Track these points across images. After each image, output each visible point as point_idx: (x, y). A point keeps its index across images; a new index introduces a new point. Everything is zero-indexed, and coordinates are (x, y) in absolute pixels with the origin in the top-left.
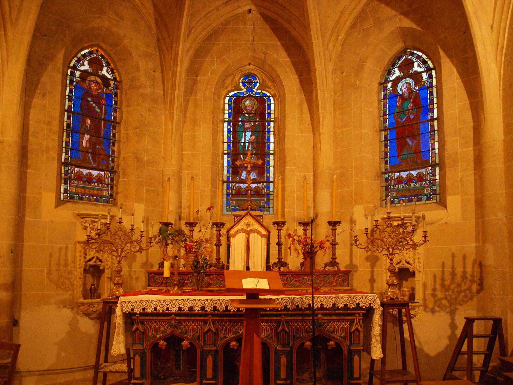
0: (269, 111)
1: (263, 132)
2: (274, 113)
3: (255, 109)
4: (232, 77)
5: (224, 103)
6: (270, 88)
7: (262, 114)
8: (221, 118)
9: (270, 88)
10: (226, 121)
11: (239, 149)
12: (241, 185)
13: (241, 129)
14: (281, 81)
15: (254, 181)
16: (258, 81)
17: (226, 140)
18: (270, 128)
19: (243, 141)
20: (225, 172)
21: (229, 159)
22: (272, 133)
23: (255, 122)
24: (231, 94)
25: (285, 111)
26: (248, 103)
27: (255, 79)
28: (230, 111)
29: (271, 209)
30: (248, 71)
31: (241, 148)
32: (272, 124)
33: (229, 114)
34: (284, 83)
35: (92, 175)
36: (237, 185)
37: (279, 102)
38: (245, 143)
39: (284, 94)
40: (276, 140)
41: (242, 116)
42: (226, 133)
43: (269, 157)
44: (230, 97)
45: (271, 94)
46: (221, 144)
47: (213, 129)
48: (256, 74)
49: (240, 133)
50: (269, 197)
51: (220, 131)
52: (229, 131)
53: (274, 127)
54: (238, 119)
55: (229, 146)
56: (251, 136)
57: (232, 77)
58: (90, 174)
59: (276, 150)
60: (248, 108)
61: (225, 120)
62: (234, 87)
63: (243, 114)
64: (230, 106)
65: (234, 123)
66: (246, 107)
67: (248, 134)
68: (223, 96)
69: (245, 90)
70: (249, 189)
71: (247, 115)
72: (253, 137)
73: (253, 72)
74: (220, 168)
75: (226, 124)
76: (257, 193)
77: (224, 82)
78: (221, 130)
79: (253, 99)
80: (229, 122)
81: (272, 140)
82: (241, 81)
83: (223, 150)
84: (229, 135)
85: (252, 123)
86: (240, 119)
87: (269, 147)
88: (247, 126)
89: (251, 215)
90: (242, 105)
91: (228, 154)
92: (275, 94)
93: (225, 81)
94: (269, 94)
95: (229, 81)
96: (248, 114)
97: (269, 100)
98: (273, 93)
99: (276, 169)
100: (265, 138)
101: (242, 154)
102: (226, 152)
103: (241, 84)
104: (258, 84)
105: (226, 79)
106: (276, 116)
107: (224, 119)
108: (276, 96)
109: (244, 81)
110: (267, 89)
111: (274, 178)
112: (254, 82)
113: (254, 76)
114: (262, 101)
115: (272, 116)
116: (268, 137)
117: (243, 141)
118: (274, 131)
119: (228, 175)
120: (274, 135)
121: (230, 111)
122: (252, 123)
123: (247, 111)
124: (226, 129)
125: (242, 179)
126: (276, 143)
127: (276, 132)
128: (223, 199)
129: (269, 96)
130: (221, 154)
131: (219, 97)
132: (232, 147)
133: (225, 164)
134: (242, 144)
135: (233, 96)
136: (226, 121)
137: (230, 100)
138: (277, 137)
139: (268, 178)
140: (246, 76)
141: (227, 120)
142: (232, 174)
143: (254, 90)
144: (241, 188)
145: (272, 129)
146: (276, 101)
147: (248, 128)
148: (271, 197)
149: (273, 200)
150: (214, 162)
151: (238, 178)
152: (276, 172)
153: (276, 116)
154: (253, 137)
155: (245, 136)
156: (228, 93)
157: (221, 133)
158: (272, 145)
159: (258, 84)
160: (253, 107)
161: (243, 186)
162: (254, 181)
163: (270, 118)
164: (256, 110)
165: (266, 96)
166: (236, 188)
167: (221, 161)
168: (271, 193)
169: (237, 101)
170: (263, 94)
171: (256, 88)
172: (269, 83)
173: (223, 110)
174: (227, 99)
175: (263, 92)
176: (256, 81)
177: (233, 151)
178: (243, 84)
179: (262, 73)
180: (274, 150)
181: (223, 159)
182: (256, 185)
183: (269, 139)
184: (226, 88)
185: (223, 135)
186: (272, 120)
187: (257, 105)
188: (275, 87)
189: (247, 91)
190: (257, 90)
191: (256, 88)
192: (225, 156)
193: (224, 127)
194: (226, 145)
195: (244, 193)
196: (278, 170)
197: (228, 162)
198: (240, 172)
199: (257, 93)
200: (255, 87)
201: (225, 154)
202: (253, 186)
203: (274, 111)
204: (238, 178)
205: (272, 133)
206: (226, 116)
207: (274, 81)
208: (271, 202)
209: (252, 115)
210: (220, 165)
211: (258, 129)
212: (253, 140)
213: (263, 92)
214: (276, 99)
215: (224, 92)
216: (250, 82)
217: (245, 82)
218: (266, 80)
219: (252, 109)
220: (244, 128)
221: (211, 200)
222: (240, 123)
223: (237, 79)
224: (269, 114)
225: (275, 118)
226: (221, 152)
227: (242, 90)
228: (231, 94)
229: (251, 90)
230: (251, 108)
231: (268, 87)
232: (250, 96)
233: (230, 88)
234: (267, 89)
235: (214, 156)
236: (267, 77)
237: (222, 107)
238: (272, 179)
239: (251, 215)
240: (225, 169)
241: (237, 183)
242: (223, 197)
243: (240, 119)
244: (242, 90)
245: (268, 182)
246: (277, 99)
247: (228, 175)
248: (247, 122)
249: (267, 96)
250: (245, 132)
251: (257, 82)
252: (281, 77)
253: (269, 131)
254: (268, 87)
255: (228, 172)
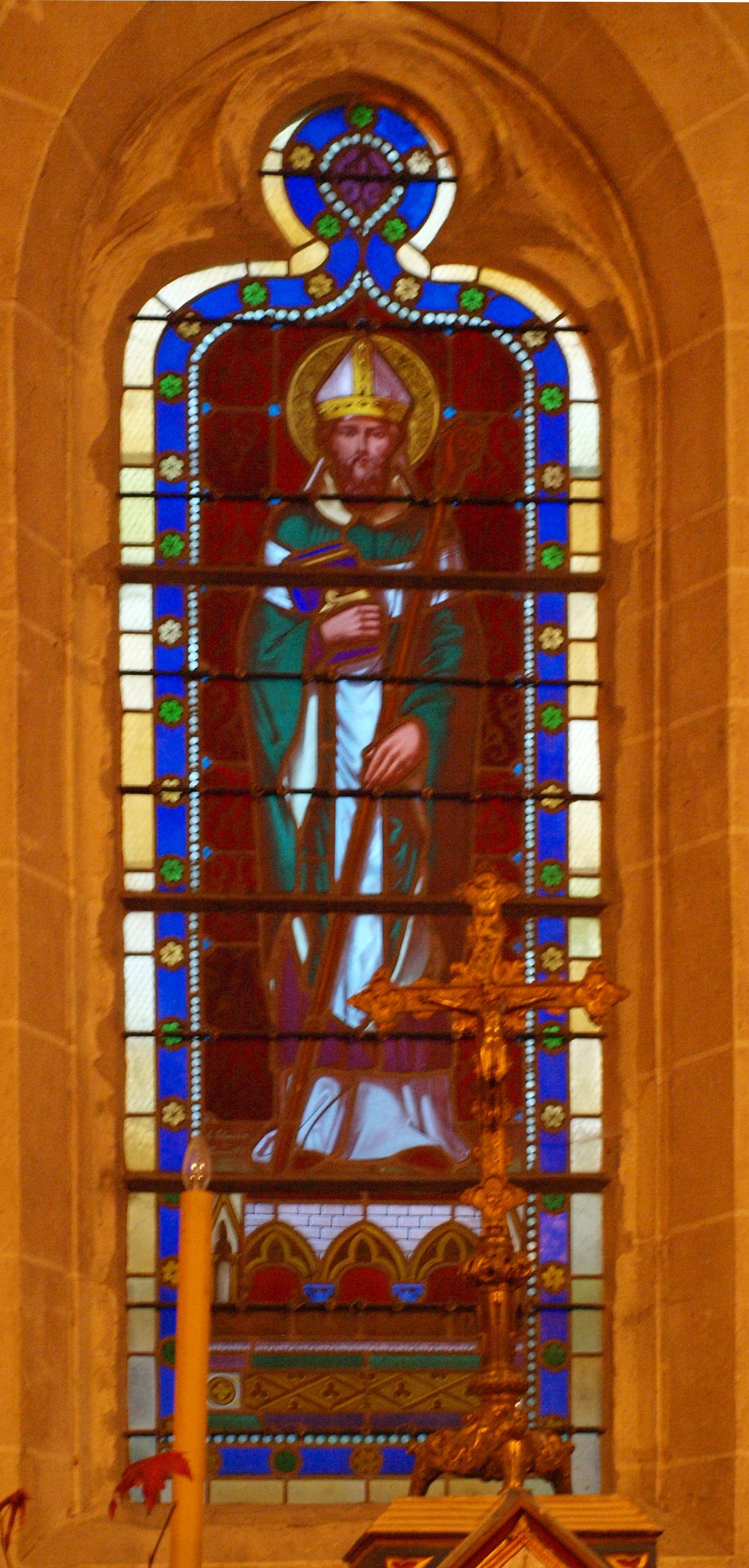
0: (552, 477)
1: (502, 688)
2: (603, 501)
3: (416, 452)
4: (188, 115)
5: (117, 389)
6: (566, 246)
7: (480, 504)
8: (93, 538)
9: (568, 247)
10: (135, 575)
11: (271, 851)
12: (302, 1217)
13: (291, 659)
14: (679, 181)
15: (417, 1178)
16: (445, 170)
17: (138, 767)
18: (561, 654)
19: (305, 774)
20: (141, 1092)
21: (173, 954)
22: (583, 700)
23: (417, 584)
24: (180, 292)
25: (718, 485)
26: (348, 387)
27: (411, 143)
28: (172, 468)
29: (585, 1448)
30: (343, 62)
31: (287, 845)
32: (582, 613)
33: (168, 499)
34: (715, 191)
35: (386, 1245)
36: (258, 1215)
37: (647, 384)
38: (324, 795)
39: (711, 312)
40: (625, 767)
41: (294, 525)
42: (138, 693)
43: (562, 942)
44: (173, 320)
45: (568, 305)
46: (98, 803)
47: (27, 647)
48: (422, 88)
49: (273, 691)
50: (563, 1335)
51: (81, 670)
52: (167, 673)
53: (605, 640)
54: (257, 548)
55: (168, 821)
56: (386, 726)
57: (188, 115)
58: (363, 1244)
59: (627, 869)
60: (349, 445)
61: (133, 557)
62: (211, 216)
63: (305, 503)
64: (168, 416)
65: (211, 583)
66: (328, 429)
67: (361, 707)
68: (102, 310)
69: (314, 256)
70: (363, 1249)
71: (336, 513)
72: (406, 740)
73: (393, 70)
74: (93, 1051)
75: (136, 604)
76: (453, 1286)
77: (112, 167)
78: (94, 661)
79: (397, 347)
80: (166, 582)
81: (584, 768)
82: (273, 162)
83: (119, 867)
84: (172, 712)
85: (395, 600)
86: (276, 554)
87: (555, 841)
88: (345, 620)
89: (546, 1533)
90: (293, 412)
91: (166, 905)
92: (613, 308)
93: (128, 155)
94: (546, 309)
95: (155, 162)
96: (347, 501)
97: (554, 372)
98: (588, 297)
99: (629, 1064)
100: (517, 750)
101: (298, 908)
102: (141, 883)
103: (274, 192)
104: (446, 195)
105: (130, 129)
106: (625, 529)
107: (115, 545)
108: (620, 328)
109: (303, 159)
110: (533, 256)
111: (612, 1148)
112: (407, 179)
113: (401, 112)
114: (482, 371)
115: (584, 526)
116: (540, 731)
117: (305, 774)
118: (605, 685)
119: (173, 1114)
120: (608, 716)
121: (172, 468)
122: (395, 600)
123: (341, 471)
124: (136, 653)
125: (310, 1159)
126: (625, 798)
127: (627, 694)
128: (124, 1355)
129: (550, 329)
130: (96, 907)
131: (69, 321)
132: (206, 836)
133: (141, 1008)
134: (300, 804)
135: (201, 311)
136: (135, 575)
137: (169, 357)
138: (630, 739)
139: (556, 1143)
140: (329, 108)
141: (145, 557)
142: (208, 1105)
143: (410, 258)
144: (297, 1243)
145: (583, 663)
146: (624, 382)
147: (352, 648)
148: (584, 1332)
149: (606, 1354)
150: (43, 991)
151: (264, 1150)
152: (631, 1090)
153: (625, 529)
154: (406, 740)
155: (329, 722)
156: (148, 287)
157: (93, 695)
158: (585, 827)
159: (446, 195)
160: (400, 440)
161: (318, 1224)
162: (417, 1178)
163: (567, 553)
164: (427, 464)
165: (524, 321)
166: (252, 1245)
167: (98, 974)
168: (582, 1292)
169: (240, 371)
170: (494, 299)
171: (425, 236)
172: (550, 194)
173: (109, 458)
174: (143, 340)
175: (495, 279)
176: (418, 165)
177: (208, 869)
178: (301, 186)
179: (481, 89)
180: (608, 870)
181: (116, 952)
182: (433, 1216)
183: (554, 761)
184: (134, 223)
185: (115, 712)
186: (581, 565)
187: (430, 417)
188: (608, 238)
189: (336, 270)
190: (435, 254)
191: (425, 236)
192: (139, 929)
193: (116, 633)
194: (139, 813)
195: (325, 1288)
196: (646, 1061)
197: (168, 981)
198: (286, 1083)
199: (431, 293)
200: (412, 230)
201: (136, 903)
202: (408, 1224)
203: (604, 477)
204: (264, 1150)
205: (583, 700)
206: (138, 521)
207: (596, 170)
208: (584, 1377)
209: (387, 516)
210: (93, 1020)
211: (451, 660)
212: (408, 768)
213: (495, 279)
214: (618, 354)
215: (113, 276)
216: (364, 177)
217: (313, 175)
218: (525, 157)
219: (388, 456)
220: (317, 647)
221: (28, 1366)
222: (279, 596)
223: (235, 132)
224: (556, 504)
225: (608, 549)
226: (96, 884)
227: (282, 250)
228: (180, 292)
229: (375, 254)
230: (376, 445)
231: (542, 233)
232: (361, 321)
233: (170, 231)
234: (533, 256)
235: (43, 911)
236: (535, 130)
237: (93, 426)
238: (586, 1158)
239: (546, 1533)
240: (141, 1056)
241: (257, 1191)
242: (123, 1335)
243: (276, 554)
244: (282, 250)
245: (555, 1183)
246: (632, 361)
247: (173, 1114)
248: (346, 583)
249: (533, 323)
250: (327, 687)
251: (432, 179)
252: (681, 136)
253: (555, 685)
254: (542, 233)
255: (170, 1084)
